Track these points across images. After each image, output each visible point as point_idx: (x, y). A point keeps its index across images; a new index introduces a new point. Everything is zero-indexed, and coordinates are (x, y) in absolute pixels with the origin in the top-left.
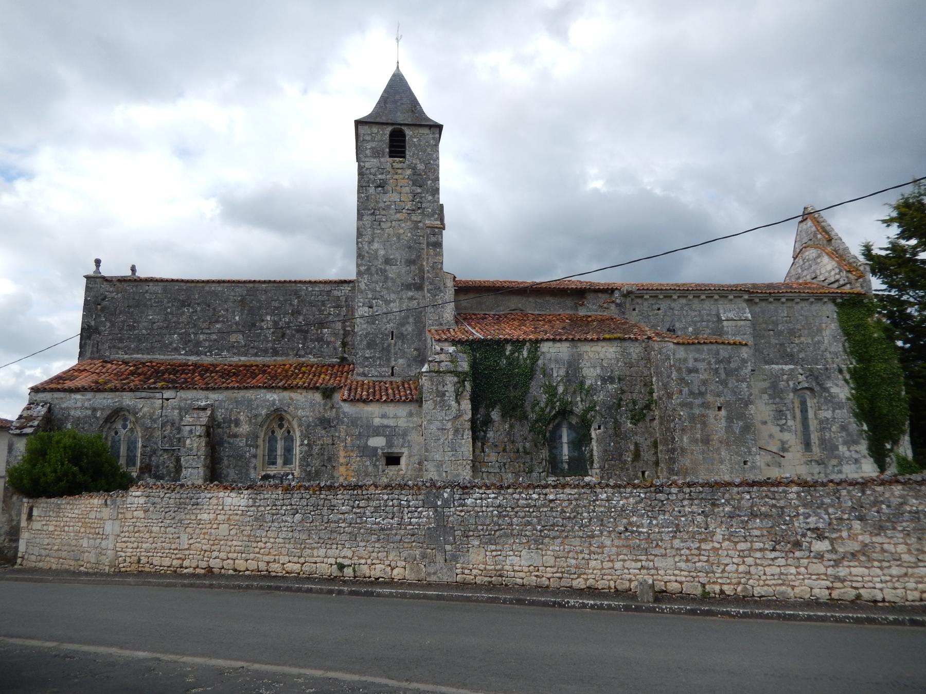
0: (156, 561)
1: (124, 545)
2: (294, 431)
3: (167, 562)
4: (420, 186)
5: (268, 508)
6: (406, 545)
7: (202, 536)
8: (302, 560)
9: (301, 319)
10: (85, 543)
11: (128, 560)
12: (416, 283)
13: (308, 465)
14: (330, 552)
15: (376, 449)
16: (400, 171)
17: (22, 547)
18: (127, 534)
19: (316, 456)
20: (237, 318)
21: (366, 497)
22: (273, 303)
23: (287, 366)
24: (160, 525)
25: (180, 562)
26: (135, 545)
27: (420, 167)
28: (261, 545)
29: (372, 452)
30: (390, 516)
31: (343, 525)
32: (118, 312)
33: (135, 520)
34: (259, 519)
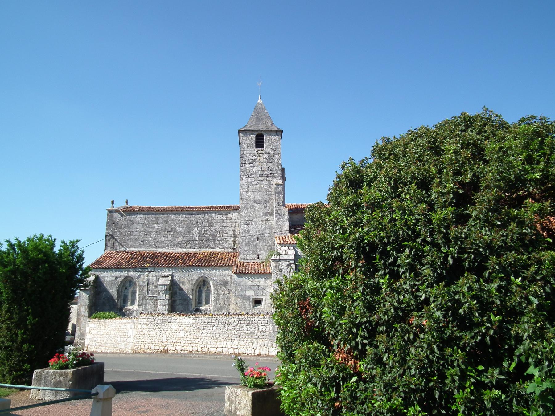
0: (152, 347)
1: (138, 340)
2: (211, 288)
3: (157, 348)
4: (271, 163)
5: (202, 324)
6: (260, 340)
7: (173, 336)
8: (216, 346)
9: (212, 229)
10: (119, 339)
11: (140, 347)
12: (269, 213)
13: (217, 304)
14: (228, 343)
15: (249, 297)
16: (261, 155)
17: (87, 343)
18: (139, 336)
19: (221, 300)
20: (181, 229)
21: (243, 319)
22: (199, 221)
23: (206, 254)
24: (154, 331)
25: (163, 347)
26: (143, 340)
27: (272, 152)
28: (198, 340)
29: (247, 298)
30: (254, 327)
31: (234, 331)
32: (123, 227)
33: (142, 329)
34: (198, 328)
